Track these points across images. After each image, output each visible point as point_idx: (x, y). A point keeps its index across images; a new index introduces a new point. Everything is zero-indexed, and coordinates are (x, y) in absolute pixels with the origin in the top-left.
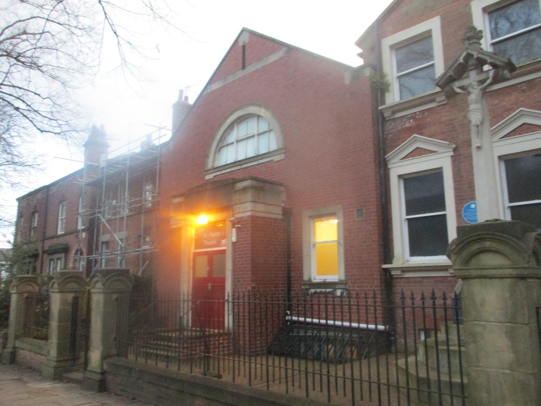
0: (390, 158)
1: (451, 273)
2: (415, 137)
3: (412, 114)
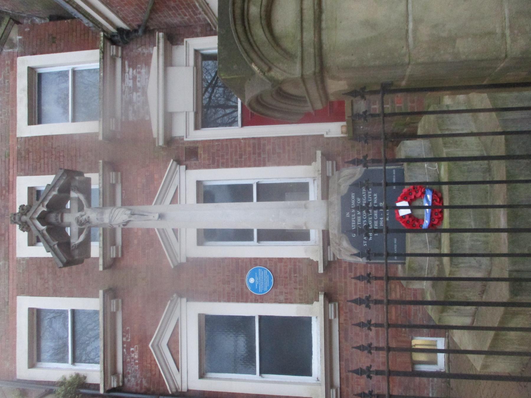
0: (173, 387)
1: (335, 317)
2: (152, 346)
3: (123, 348)
